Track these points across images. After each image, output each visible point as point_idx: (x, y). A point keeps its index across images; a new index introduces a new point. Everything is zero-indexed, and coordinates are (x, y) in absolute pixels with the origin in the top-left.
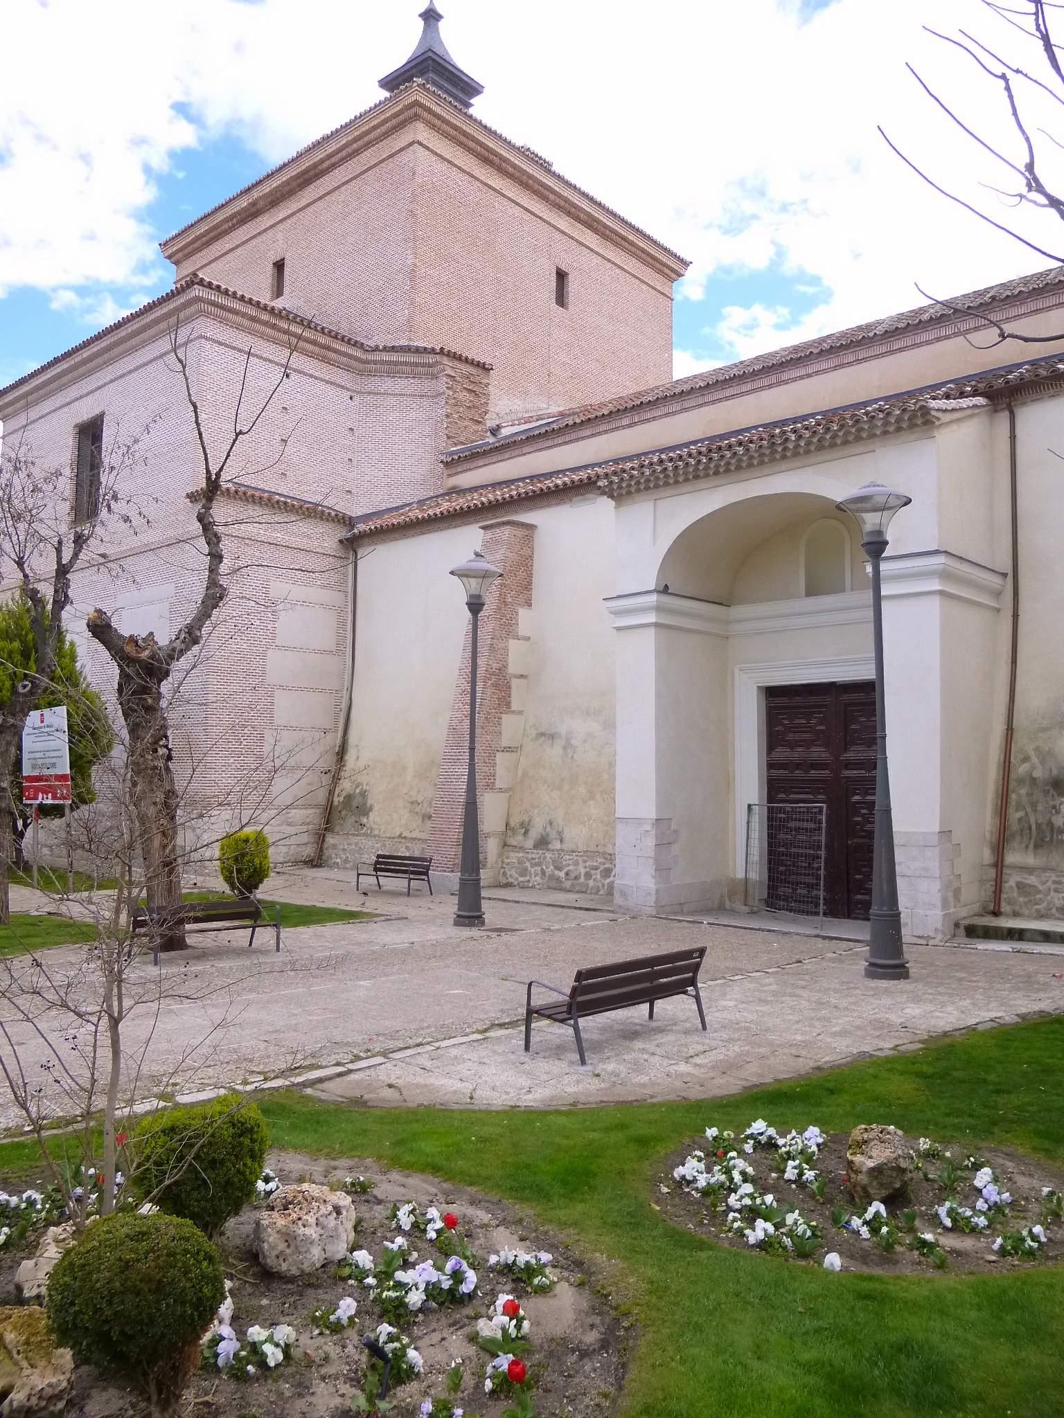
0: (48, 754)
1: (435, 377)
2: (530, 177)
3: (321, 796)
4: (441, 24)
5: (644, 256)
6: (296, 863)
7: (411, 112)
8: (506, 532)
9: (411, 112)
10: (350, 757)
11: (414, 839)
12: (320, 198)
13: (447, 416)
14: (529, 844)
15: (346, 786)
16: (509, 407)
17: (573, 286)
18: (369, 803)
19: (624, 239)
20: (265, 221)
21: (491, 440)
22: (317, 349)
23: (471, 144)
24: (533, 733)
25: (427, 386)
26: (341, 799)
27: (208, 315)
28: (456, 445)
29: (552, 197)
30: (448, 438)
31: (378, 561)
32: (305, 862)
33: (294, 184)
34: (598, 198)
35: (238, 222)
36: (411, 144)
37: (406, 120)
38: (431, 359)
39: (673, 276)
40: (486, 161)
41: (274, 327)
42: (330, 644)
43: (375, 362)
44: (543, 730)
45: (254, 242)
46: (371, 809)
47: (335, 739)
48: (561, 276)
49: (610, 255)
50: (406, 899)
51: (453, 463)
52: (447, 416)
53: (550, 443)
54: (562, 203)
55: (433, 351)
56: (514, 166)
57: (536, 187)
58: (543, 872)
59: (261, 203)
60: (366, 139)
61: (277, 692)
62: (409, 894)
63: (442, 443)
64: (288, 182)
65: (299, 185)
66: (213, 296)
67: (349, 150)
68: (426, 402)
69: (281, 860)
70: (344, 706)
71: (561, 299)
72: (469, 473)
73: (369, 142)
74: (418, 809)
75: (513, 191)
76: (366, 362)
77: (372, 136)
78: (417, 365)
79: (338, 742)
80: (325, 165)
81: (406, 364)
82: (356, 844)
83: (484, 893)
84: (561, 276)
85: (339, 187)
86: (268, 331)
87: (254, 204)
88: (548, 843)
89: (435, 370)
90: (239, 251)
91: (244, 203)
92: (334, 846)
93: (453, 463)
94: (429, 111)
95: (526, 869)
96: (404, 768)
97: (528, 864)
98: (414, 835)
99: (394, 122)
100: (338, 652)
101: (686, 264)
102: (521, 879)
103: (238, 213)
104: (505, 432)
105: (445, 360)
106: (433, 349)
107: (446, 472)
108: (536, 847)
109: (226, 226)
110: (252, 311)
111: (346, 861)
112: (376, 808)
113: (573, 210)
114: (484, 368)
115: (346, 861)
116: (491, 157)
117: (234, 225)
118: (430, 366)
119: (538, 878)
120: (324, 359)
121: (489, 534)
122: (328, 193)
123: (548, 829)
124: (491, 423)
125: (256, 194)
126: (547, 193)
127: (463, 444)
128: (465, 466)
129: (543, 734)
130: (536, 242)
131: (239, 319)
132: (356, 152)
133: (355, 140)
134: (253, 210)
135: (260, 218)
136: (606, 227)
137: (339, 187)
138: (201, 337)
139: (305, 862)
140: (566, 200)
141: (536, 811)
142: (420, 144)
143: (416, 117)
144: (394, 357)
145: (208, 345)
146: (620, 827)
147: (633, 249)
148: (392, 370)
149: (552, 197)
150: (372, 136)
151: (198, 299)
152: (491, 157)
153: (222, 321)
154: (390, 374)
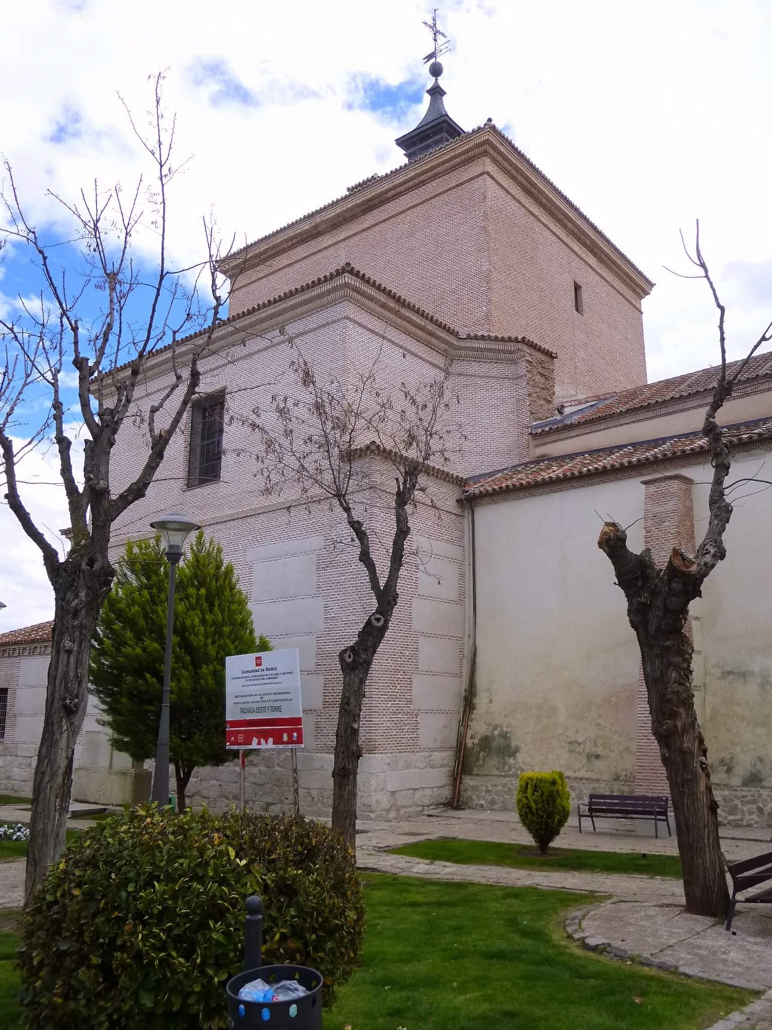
0: (266, 698)
1: (514, 362)
2: (558, 208)
3: (453, 742)
4: (445, 98)
5: (625, 277)
6: (438, 805)
7: (481, 149)
8: (675, 485)
9: (481, 149)
10: (481, 701)
11: (581, 779)
12: (384, 221)
13: (529, 395)
14: (736, 781)
15: (479, 728)
16: (571, 393)
17: (585, 295)
18: (513, 744)
19: (614, 262)
20: (326, 240)
21: (559, 417)
22: (424, 335)
23: (521, 179)
24: (718, 672)
25: (509, 370)
26: (476, 741)
27: (350, 299)
28: (536, 420)
29: (569, 225)
30: (532, 413)
31: (489, 517)
32: (444, 805)
33: (358, 210)
34: (600, 228)
35: (297, 243)
36: (483, 173)
37: (475, 156)
38: (512, 346)
39: (642, 294)
40: (528, 192)
41: (397, 313)
42: (454, 595)
43: (465, 349)
44: (730, 669)
45: (315, 258)
46: (517, 750)
47: (460, 685)
48: (577, 288)
49: (605, 275)
50: (655, 840)
51: (537, 436)
52: (529, 395)
53: (651, 414)
54: (576, 230)
55: (516, 340)
56: (547, 198)
57: (560, 216)
58: (760, 810)
59: (323, 227)
60: (435, 171)
61: (421, 639)
62: (657, 837)
63: (526, 419)
64: (352, 209)
65: (362, 211)
66: (357, 283)
67: (416, 181)
68: (507, 383)
69: (427, 803)
70: (467, 651)
71: (578, 307)
72: (558, 443)
73: (436, 175)
74: (580, 749)
75: (545, 218)
76: (460, 348)
77: (440, 169)
78: (500, 351)
79: (465, 684)
80: (390, 194)
81: (491, 350)
82: (504, 785)
83: (722, 832)
84: (577, 288)
85: (405, 211)
86: (392, 316)
87: (316, 227)
88: (761, 780)
89: (515, 356)
90: (298, 266)
91: (306, 226)
92: (475, 788)
93: (537, 436)
94: (495, 148)
95: (736, 807)
96: (554, 709)
97: (737, 802)
98: (579, 774)
99: (463, 157)
100: (461, 601)
101: (652, 285)
102: (731, 818)
103: (300, 234)
104: (567, 411)
105: (525, 348)
106: (516, 338)
107: (532, 443)
108: (744, 784)
109: (286, 246)
110: (383, 298)
111: (493, 802)
112: (524, 749)
113: (582, 237)
114: (551, 356)
115: (493, 802)
116: (533, 189)
117: (293, 245)
118: (510, 352)
119: (753, 816)
120: (428, 344)
121: (652, 488)
122: (393, 216)
123: (759, 766)
124: (557, 402)
125: (318, 219)
126: (566, 221)
127: (540, 419)
128: (555, 437)
129: (730, 673)
130: (560, 261)
131: (373, 305)
132: (423, 183)
133: (423, 173)
134: (314, 232)
135: (320, 239)
136: (603, 251)
137: (405, 211)
138: (347, 318)
139: (444, 805)
140: (579, 228)
141: (738, 748)
142: (488, 173)
143: (485, 153)
144: (482, 345)
145: (351, 325)
146: (30, 796)
147: (619, 271)
148: (479, 356)
149: (569, 225)
150: (440, 169)
151: (346, 285)
152: (533, 189)
153: (362, 306)
154: (476, 359)
